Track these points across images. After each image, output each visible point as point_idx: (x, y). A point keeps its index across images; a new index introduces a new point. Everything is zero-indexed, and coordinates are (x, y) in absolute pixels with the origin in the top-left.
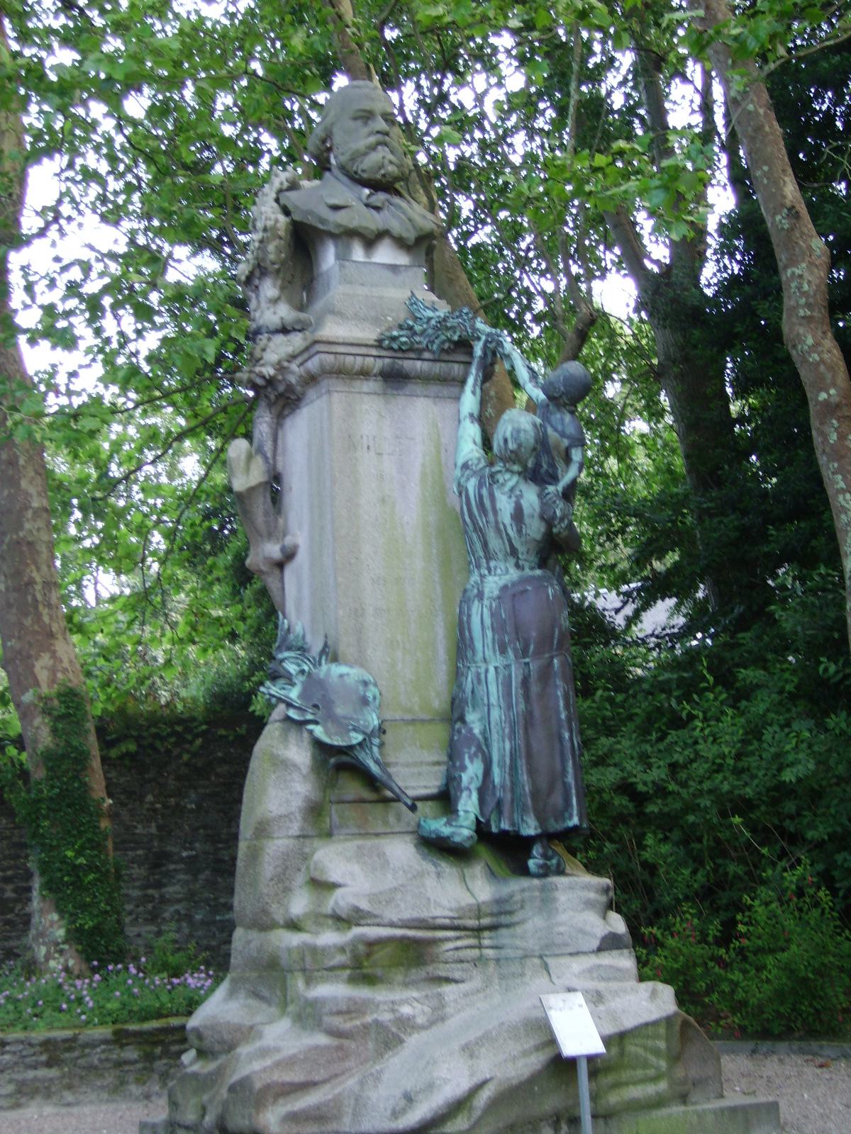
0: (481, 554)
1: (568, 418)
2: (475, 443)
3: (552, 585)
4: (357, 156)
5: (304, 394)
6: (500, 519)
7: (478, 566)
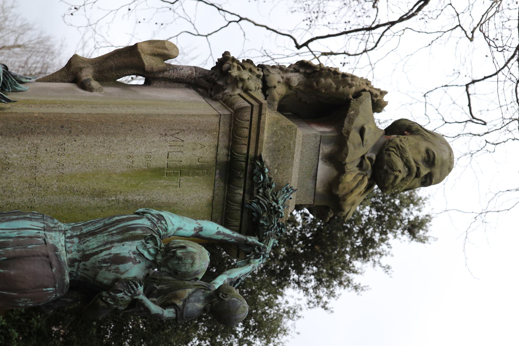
0: (84, 231)
1: (200, 306)
2: (179, 229)
3: (55, 291)
4: (401, 151)
5: (216, 100)
7: (73, 229)
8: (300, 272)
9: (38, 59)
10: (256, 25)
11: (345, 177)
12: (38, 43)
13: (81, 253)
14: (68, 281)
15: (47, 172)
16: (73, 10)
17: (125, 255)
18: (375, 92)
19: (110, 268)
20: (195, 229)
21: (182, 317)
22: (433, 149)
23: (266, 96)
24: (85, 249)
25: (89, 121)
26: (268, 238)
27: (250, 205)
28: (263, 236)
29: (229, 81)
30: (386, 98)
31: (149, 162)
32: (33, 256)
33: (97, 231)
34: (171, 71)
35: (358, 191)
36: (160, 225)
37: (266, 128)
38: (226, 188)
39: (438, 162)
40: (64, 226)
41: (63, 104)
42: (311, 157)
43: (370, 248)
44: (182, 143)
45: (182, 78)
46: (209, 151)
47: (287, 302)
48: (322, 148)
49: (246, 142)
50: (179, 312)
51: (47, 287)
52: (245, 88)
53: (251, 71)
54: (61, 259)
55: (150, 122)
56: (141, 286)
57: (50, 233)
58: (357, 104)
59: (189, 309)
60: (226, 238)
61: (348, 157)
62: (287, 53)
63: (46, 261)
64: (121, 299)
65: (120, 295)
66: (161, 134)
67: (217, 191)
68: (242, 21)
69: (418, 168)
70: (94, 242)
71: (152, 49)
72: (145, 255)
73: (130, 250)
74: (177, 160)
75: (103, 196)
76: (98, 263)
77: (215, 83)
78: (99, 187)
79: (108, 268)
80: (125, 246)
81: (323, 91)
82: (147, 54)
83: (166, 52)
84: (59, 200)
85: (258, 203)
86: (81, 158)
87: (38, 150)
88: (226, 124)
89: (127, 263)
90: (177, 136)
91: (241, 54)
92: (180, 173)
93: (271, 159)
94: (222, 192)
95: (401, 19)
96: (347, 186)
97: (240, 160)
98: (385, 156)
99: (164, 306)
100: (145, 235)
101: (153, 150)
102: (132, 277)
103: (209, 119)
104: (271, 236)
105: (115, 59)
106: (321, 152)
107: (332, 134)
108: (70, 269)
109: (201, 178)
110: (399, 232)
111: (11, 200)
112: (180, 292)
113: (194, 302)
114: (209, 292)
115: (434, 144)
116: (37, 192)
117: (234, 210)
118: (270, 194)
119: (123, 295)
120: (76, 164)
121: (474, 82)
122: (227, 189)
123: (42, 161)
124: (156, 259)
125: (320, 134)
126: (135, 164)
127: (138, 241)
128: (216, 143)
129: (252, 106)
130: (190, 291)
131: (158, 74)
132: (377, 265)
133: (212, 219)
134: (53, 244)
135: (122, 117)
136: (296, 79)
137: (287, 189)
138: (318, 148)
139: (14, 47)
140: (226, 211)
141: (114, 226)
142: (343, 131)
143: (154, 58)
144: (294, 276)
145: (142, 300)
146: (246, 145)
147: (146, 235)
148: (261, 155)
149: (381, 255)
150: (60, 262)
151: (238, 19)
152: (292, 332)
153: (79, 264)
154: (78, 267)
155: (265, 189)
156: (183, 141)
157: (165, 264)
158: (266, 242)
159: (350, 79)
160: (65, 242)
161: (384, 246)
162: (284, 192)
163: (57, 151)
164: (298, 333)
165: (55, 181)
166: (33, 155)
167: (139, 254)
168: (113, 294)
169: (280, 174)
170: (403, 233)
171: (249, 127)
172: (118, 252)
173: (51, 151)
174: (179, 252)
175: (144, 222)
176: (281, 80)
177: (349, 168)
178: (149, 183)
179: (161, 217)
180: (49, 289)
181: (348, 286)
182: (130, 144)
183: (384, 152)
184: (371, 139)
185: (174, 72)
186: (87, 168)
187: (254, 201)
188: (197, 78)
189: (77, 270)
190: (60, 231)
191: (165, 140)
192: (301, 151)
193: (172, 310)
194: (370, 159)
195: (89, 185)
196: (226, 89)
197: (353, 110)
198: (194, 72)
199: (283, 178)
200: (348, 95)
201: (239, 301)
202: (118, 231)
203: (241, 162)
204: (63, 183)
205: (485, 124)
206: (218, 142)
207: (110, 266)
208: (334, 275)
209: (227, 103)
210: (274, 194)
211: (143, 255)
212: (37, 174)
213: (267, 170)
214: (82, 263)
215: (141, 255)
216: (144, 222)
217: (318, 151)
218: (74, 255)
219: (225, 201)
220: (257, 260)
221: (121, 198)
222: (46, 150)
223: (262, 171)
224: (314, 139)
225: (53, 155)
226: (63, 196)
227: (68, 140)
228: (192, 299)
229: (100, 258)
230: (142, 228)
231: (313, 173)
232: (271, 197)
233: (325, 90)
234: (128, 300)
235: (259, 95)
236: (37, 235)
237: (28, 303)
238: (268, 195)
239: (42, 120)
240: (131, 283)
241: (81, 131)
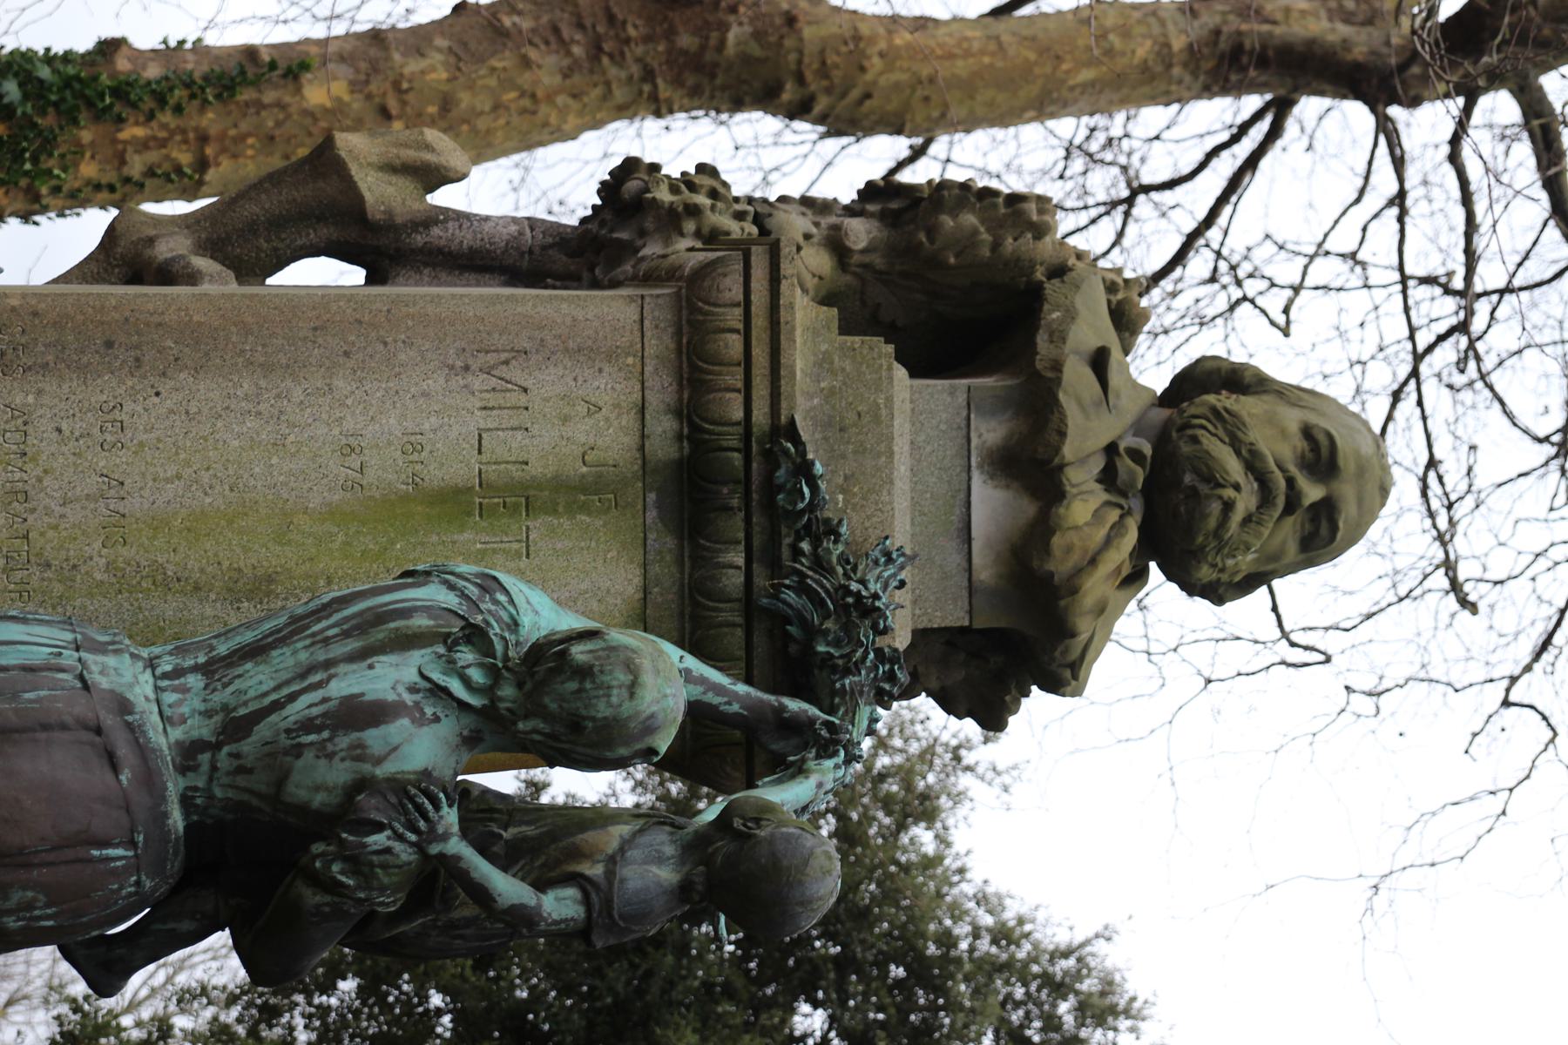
0: (222, 649)
1: (666, 875)
3: (136, 866)
6: (342, 668)
11: (1067, 508)
13: (218, 718)
14: (180, 826)
15: (67, 510)
17: (381, 696)
19: (330, 747)
21: (611, 916)
22: (1313, 419)
24: (233, 702)
25: (200, 324)
27: (776, 597)
28: (834, 693)
29: (649, 224)
31: (418, 467)
32: (46, 727)
33: (270, 640)
34: (450, 224)
36: (493, 608)
38: (686, 554)
39: (1346, 461)
42: (945, 462)
44: (523, 400)
45: (488, 251)
46: (616, 423)
48: (977, 429)
50: (594, 896)
51: (106, 844)
52: (706, 230)
54: (149, 740)
55: (410, 323)
56: (450, 806)
57: (100, 658)
58: (1064, 291)
61: (1068, 441)
63: (92, 744)
64: (382, 858)
65: (379, 840)
66: (452, 367)
67: (655, 569)
70: (261, 677)
71: (383, 149)
72: (452, 690)
73: (397, 682)
74: (513, 459)
75: (268, 594)
76: (283, 735)
78: (253, 561)
79: (324, 748)
80: (378, 670)
81: (952, 260)
82: (369, 164)
83: (429, 157)
84: (116, 613)
85: (802, 588)
86: (182, 456)
87: (30, 429)
88: (665, 329)
89: (393, 722)
90: (503, 371)
92: (527, 507)
93: (821, 452)
94: (674, 569)
96: (1076, 541)
97: (725, 444)
98: (1181, 444)
100: (444, 630)
101: (427, 426)
102: (415, 773)
103: (606, 310)
104: (861, 693)
105: (263, 196)
106: (975, 442)
108: (182, 783)
109: (599, 523)
113: (645, 862)
116: (36, 585)
117: (721, 625)
118: (834, 560)
119: (389, 838)
120: (168, 480)
122: (690, 557)
123: (46, 472)
124: (494, 700)
126: (371, 476)
127: (423, 651)
128: (637, 396)
131: (409, 235)
134: (112, 691)
135: (314, 308)
136: (860, 232)
138: (964, 432)
140: (692, 633)
141: (327, 617)
142: (1039, 365)
143: (394, 179)
145: (457, 858)
146: (738, 391)
147: (448, 630)
148: (792, 422)
150: (143, 750)
153: (213, 756)
154: (214, 768)
155: (816, 543)
156: (525, 390)
158: (846, 712)
160: (157, 688)
162: (876, 562)
163: (96, 431)
165: (97, 545)
166: (14, 447)
167: (430, 690)
168: (351, 838)
169: (853, 509)
171: (741, 326)
172: (355, 690)
173: (77, 434)
175: (435, 594)
177: (1074, 481)
178: (422, 544)
179: (494, 585)
180: (111, 852)
182: (349, 402)
183: (1174, 435)
185: (460, 226)
186: (206, 494)
187: (787, 582)
188: (537, 250)
189: (211, 779)
191: (466, 386)
192: (912, 443)
193: (571, 892)
195: (216, 555)
196: (644, 245)
197: (1057, 307)
198: (528, 231)
199: (867, 524)
201: (809, 836)
202: (345, 627)
203: (730, 454)
206: (643, 390)
207: (330, 739)
210: (848, 562)
211: (446, 691)
212: (31, 519)
214: (226, 750)
216: (435, 594)
217: (964, 441)
218: (192, 727)
219: (687, 602)
220: (829, 763)
222: (59, 430)
224: (949, 399)
225: (84, 448)
226: (127, 600)
227: (133, 394)
228: (633, 854)
229: (292, 719)
230: (428, 610)
231: (956, 517)
232: (840, 570)
233: (957, 256)
234: (410, 863)
236: (53, 661)
237: (37, 913)
238: (829, 562)
239: (37, 322)
240: (413, 791)
241: (176, 360)
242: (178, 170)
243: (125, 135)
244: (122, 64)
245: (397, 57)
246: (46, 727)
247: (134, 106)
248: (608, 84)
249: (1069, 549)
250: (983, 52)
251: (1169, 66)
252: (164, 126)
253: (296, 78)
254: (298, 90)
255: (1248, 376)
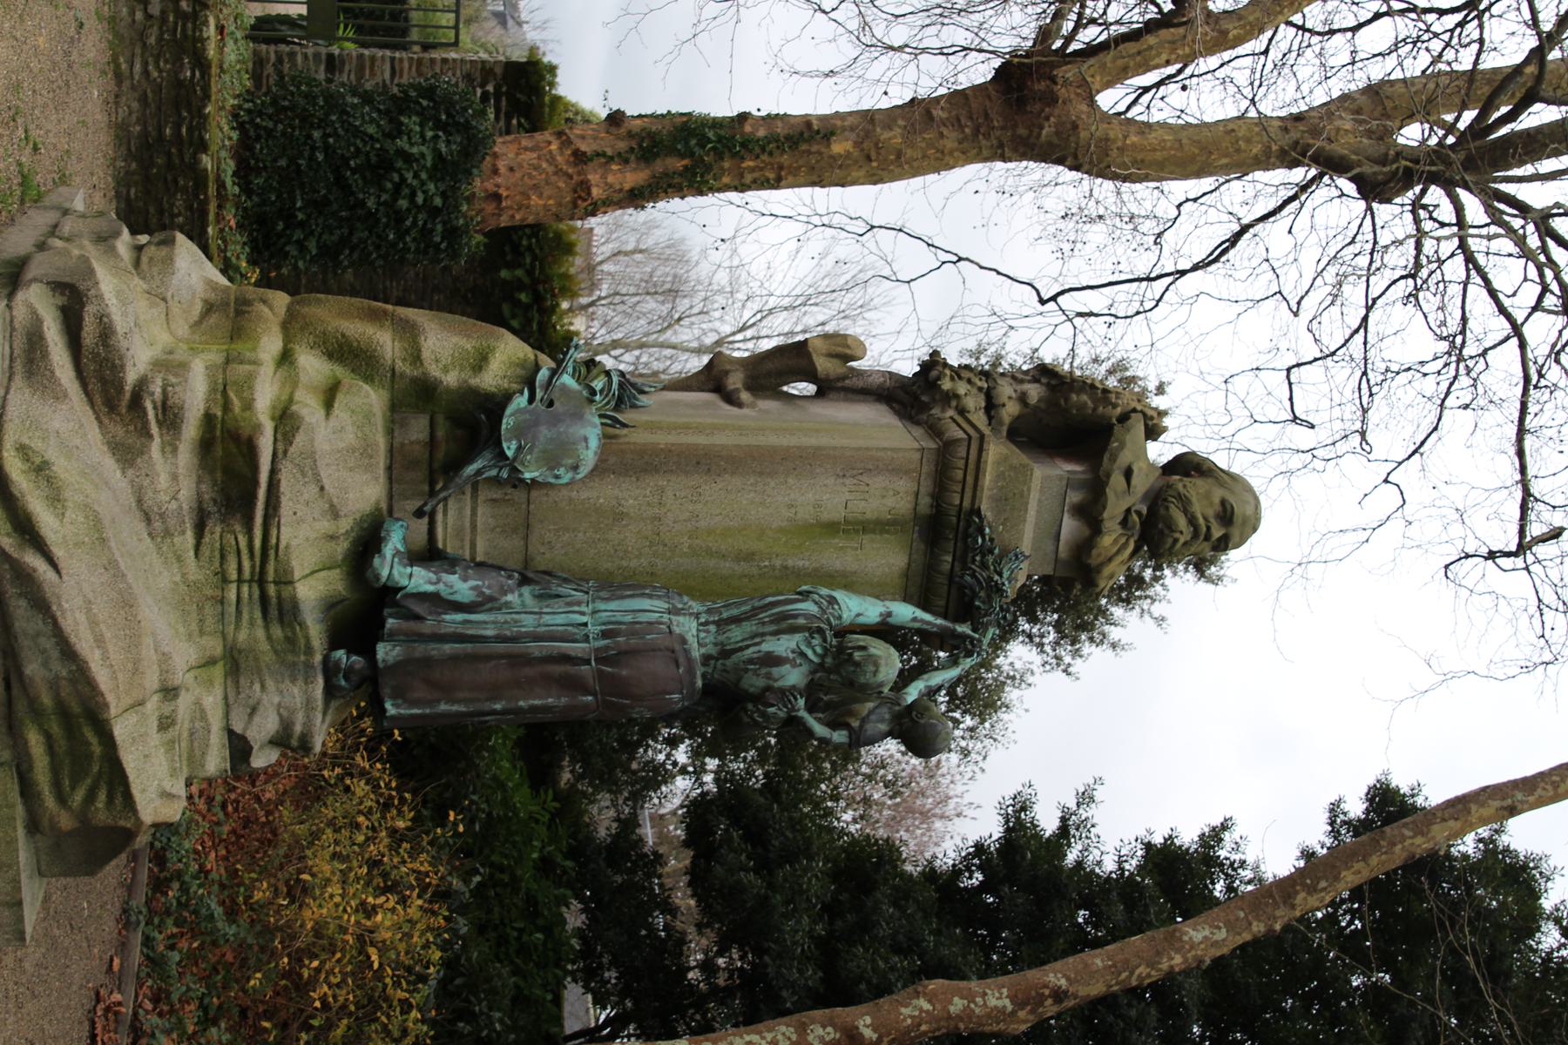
0: (725, 615)
2: (858, 615)
3: (682, 700)
5: (918, 423)
6: (768, 638)
7: (709, 611)
8: (1033, 620)
9: (668, 269)
10: (982, 267)
12: (668, 247)
16: (719, 242)
18: (1150, 413)
20: (881, 615)
22: (1231, 499)
23: (990, 418)
26: (986, 627)
29: (937, 397)
30: (1166, 421)
32: (654, 650)
35: (1120, 558)
37: (989, 468)
39: (1238, 519)
40: (696, 606)
41: (700, 429)
43: (1137, 590)
47: (1012, 664)
49: (958, 488)
53: (969, 381)
59: (869, 733)
60: (925, 626)
62: (1026, 312)
67: (915, 556)
68: (962, 263)
69: (1208, 528)
77: (916, 398)
80: (781, 642)
83: (848, 352)
85: (973, 576)
90: (860, 477)
91: (958, 311)
95: (1195, 268)
99: (834, 725)
107: (1083, 476)
108: (703, 669)
110: (1181, 567)
111: (625, 563)
112: (857, 707)
114: (897, 708)
115: (1232, 492)
121: (1298, 365)
125: (1066, 475)
126: (799, 516)
129: (970, 437)
130: (870, 705)
132: (1146, 616)
133: (906, 599)
136: (1034, 392)
137: (1016, 556)
139: (634, 252)
142: (1101, 473)
144: (1024, 625)
145: (802, 718)
149: (1153, 601)
150: (689, 660)
151: (955, 259)
152: (1017, 709)
155: (983, 556)
157: (836, 669)
159: (1113, 396)
160: (698, 630)
161: (1158, 588)
164: (1027, 711)
170: (1186, 570)
172: (771, 649)
174: (857, 655)
175: (809, 607)
176: (1014, 395)
181: (1102, 642)
184: (1141, 483)
190: (691, 614)
193: (845, 733)
194: (1139, 513)
200: (1111, 418)
204: (697, 541)
205: (1313, 427)
208: (1087, 627)
209: (934, 430)
213: (987, 530)
215: (803, 655)
216: (809, 607)
220: (969, 660)
221: (778, 563)
223: (981, 531)
228: (873, 717)
235: (980, 419)
242: (768, 180)
243: (744, 165)
244: (748, 128)
245: (878, 130)
246: (654, 650)
247: (750, 151)
248: (980, 148)
249: (1099, 555)
250: (1171, 148)
251: (1269, 158)
252: (763, 161)
253: (828, 139)
254: (829, 146)
255: (1205, 467)
